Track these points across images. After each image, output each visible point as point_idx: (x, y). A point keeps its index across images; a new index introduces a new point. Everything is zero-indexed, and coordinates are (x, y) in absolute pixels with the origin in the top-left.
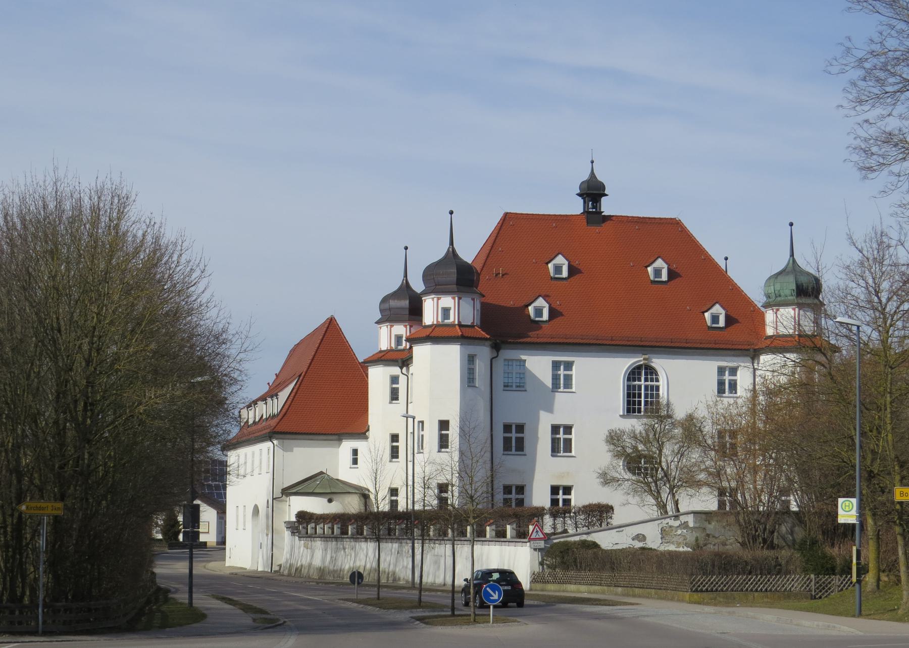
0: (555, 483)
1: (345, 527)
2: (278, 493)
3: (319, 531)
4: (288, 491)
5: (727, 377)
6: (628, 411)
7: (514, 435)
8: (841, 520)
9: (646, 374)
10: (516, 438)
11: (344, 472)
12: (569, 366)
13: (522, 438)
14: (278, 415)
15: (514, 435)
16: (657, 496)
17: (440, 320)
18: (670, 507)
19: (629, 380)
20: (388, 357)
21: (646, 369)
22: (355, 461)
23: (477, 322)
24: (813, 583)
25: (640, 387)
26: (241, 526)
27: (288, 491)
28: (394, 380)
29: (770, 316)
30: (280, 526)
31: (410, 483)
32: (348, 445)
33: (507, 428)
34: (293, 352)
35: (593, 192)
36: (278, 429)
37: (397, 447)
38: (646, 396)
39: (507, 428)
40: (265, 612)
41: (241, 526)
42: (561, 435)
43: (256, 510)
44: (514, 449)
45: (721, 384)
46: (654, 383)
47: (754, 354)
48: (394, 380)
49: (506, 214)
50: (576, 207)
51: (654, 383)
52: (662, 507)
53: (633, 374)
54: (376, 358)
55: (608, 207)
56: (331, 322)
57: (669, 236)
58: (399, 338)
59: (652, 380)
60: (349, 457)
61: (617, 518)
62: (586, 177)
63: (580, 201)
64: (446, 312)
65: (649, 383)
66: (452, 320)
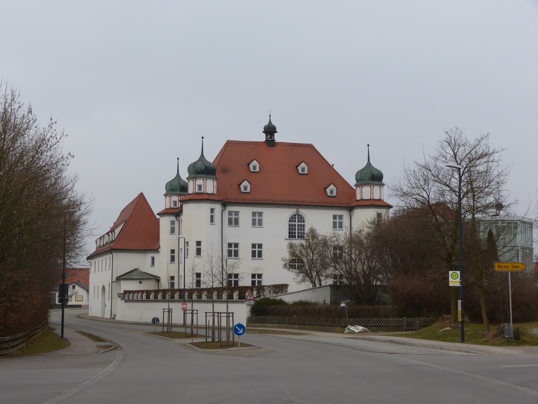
1: (148, 296)
2: (114, 280)
3: (135, 298)
4: (119, 279)
6: (289, 237)
7: (233, 249)
8: (451, 284)
9: (298, 218)
10: (235, 250)
12: (260, 214)
13: (237, 250)
14: (115, 240)
15: (233, 249)
16: (311, 278)
18: (317, 282)
19: (290, 221)
20: (169, 211)
22: (153, 263)
23: (215, 192)
24: (405, 322)
25: (295, 225)
26: (96, 296)
29: (358, 190)
30: (115, 295)
31: (182, 273)
32: (149, 256)
33: (230, 245)
34: (122, 212)
35: (270, 130)
36: (114, 248)
37: (174, 256)
38: (298, 229)
39: (230, 245)
40: (103, 341)
41: (96, 296)
43: (104, 288)
44: (257, 224)
45: (335, 223)
46: (302, 223)
47: (350, 209)
48: (173, 223)
49: (228, 141)
50: (262, 138)
51: (302, 223)
52: (313, 283)
53: (292, 219)
54: (163, 212)
55: (278, 138)
56: (141, 195)
57: (308, 151)
58: (175, 203)
59: (301, 222)
61: (290, 289)
62: (266, 123)
63: (264, 135)
64: (200, 187)
65: (300, 223)
66: (202, 191)
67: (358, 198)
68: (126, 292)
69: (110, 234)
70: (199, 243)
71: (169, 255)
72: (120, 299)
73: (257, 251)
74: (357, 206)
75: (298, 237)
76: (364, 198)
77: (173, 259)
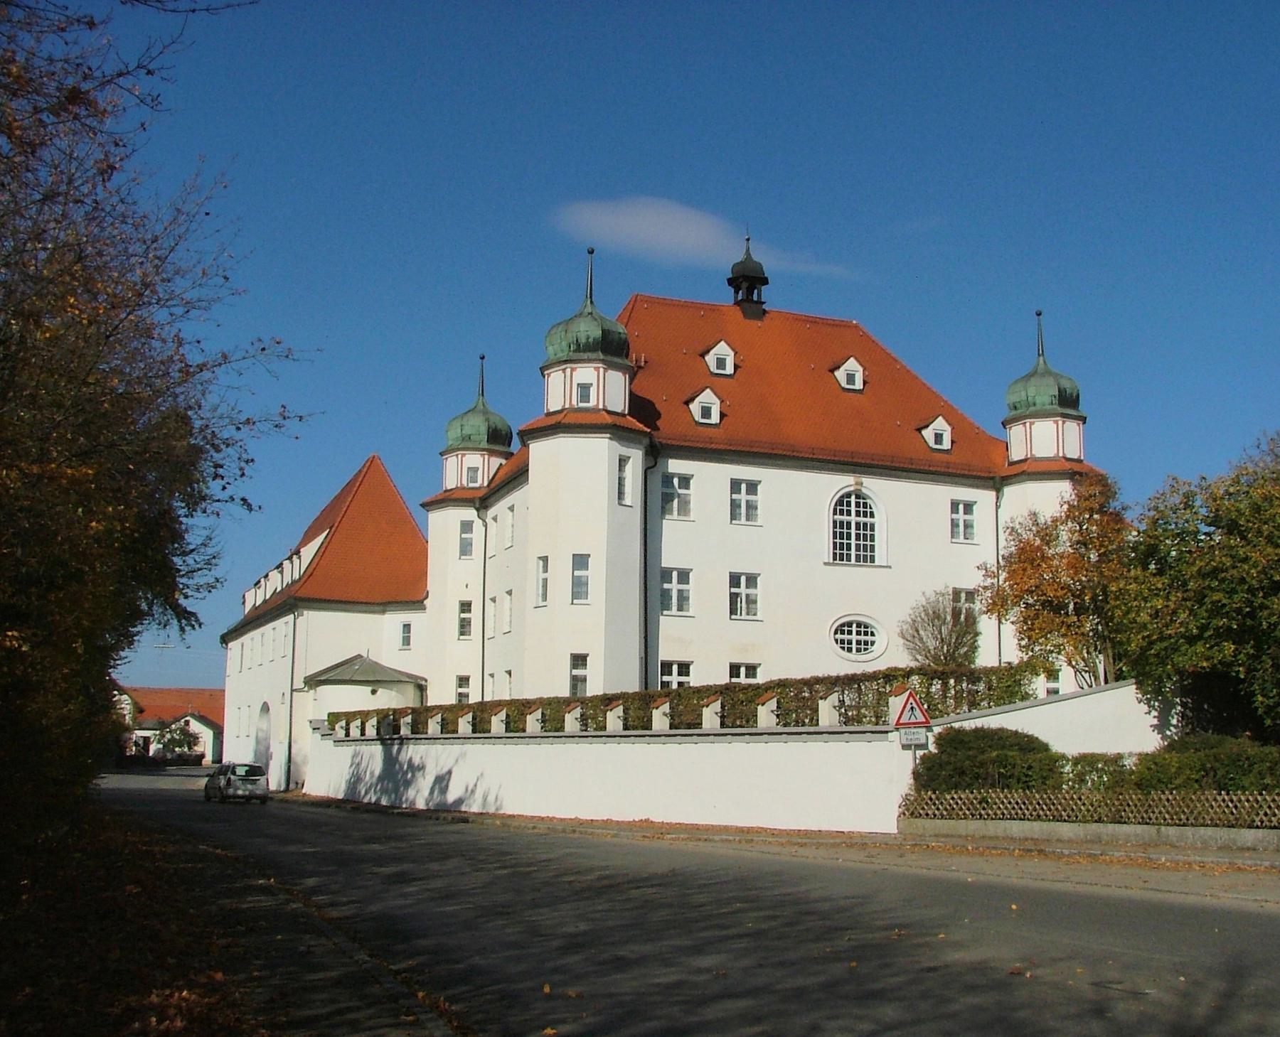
0: (736, 660)
2: (299, 684)
4: (314, 681)
5: (743, 590)
9: (858, 505)
11: (391, 657)
12: (752, 487)
17: (574, 402)
21: (858, 497)
22: (407, 641)
27: (314, 681)
28: (467, 527)
32: (392, 621)
42: (743, 590)
46: (868, 520)
48: (467, 527)
51: (868, 520)
53: (841, 504)
59: (865, 515)
60: (399, 634)
62: (740, 257)
64: (584, 389)
66: (593, 403)
67: (1017, 453)
68: (334, 718)
69: (287, 564)
70: (580, 561)
71: (454, 616)
72: (318, 736)
73: (741, 593)
74: (1023, 473)
75: (858, 558)
76: (1038, 455)
77: (464, 627)
